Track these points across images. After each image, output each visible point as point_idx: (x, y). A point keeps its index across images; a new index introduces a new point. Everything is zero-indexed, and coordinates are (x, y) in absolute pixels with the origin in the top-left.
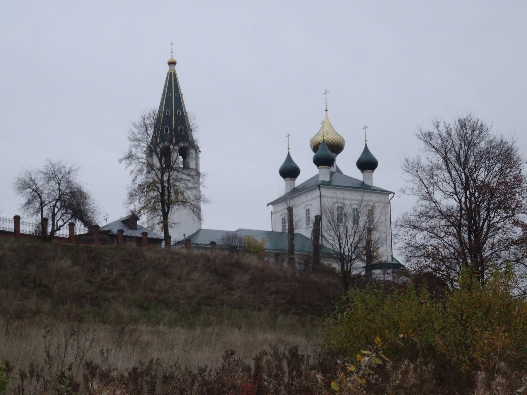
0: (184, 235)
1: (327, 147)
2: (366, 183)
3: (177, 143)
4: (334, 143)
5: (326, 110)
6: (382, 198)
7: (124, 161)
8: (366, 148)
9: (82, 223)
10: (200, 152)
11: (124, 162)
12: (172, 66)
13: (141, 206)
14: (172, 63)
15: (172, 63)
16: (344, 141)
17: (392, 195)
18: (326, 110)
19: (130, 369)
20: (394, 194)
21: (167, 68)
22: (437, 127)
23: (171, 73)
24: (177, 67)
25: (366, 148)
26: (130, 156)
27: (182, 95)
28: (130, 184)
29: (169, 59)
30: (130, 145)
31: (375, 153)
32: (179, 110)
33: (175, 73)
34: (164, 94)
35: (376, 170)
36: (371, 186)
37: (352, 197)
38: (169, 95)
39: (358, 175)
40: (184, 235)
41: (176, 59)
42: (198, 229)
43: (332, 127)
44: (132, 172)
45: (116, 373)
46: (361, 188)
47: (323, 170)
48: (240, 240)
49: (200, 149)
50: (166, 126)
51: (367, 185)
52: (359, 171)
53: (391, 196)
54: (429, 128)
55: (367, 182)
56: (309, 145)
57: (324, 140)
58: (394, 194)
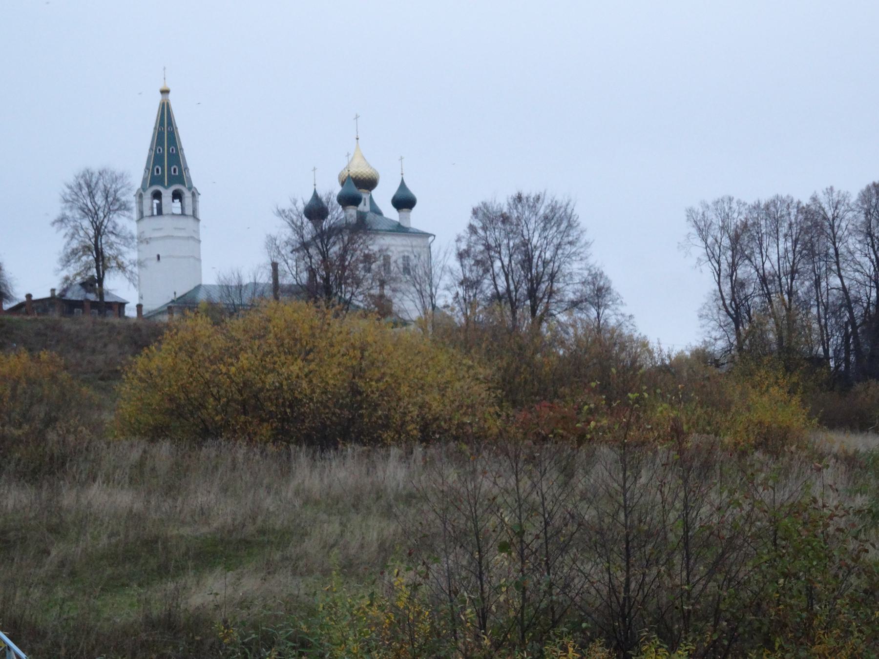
0: (175, 293)
1: (352, 183)
2: (402, 224)
3: (170, 183)
4: (360, 178)
5: (357, 139)
6: (417, 242)
7: (56, 224)
9: (326, 204)
12: (165, 95)
13: (75, 272)
14: (165, 92)
15: (165, 92)
18: (357, 139)
20: (434, 236)
21: (159, 97)
22: (295, 204)
24: (171, 97)
26: (62, 220)
27: (176, 128)
28: (62, 248)
29: (161, 86)
31: (414, 189)
32: (175, 166)
33: (168, 104)
35: (414, 209)
38: (159, 150)
39: (391, 213)
40: (175, 293)
41: (169, 86)
42: (197, 284)
43: (365, 159)
44: (65, 236)
45: (547, 369)
46: (397, 231)
49: (199, 192)
50: (157, 167)
51: (403, 227)
53: (431, 239)
55: (404, 224)
57: (349, 175)
58: (434, 236)
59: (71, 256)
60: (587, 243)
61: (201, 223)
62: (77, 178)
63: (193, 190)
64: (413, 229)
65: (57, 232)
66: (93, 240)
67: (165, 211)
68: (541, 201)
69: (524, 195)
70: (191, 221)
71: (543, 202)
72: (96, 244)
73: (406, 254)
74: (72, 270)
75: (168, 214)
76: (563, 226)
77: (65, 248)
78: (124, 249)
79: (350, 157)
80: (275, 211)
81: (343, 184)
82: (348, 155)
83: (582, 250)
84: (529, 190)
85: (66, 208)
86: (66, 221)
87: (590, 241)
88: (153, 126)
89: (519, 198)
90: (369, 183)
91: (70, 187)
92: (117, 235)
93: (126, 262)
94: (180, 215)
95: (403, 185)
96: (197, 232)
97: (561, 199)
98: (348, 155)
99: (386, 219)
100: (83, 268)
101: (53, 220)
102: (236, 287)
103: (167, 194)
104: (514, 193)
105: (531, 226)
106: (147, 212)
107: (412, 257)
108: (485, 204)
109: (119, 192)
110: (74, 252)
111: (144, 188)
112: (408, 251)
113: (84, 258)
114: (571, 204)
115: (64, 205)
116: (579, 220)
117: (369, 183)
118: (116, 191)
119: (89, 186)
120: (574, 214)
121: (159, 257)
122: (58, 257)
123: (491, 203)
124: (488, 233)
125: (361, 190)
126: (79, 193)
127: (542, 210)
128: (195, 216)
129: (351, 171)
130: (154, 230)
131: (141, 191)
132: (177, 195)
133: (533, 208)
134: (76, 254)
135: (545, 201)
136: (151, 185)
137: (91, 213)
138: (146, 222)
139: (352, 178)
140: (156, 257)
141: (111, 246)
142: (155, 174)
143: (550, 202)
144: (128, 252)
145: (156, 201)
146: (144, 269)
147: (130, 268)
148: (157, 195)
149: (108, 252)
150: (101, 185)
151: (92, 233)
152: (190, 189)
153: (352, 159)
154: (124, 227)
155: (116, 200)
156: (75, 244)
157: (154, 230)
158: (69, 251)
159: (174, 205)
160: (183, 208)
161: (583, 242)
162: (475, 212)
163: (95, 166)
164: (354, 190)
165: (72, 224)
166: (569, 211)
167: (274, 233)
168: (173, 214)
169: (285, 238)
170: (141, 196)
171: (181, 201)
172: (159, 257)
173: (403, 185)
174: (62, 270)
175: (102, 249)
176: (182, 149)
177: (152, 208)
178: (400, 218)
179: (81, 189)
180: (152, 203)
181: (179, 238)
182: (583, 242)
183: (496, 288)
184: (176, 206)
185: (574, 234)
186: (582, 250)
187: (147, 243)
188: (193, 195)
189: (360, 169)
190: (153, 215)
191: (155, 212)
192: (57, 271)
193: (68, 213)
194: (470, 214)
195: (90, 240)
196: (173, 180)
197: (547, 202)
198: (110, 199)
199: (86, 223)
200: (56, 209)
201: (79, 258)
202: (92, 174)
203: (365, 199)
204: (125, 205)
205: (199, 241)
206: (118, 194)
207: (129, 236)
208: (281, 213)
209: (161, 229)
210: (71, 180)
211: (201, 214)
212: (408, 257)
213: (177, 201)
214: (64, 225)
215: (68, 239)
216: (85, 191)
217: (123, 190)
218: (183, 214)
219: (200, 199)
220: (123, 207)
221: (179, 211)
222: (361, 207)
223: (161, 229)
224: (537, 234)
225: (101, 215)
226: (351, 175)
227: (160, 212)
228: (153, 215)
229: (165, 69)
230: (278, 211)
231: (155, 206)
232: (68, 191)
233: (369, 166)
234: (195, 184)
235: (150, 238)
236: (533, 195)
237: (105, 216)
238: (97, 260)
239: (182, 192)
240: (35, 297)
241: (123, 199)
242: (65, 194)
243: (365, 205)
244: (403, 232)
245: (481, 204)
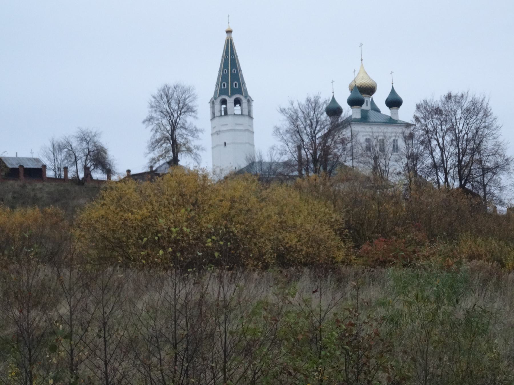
2: (392, 118)
3: (233, 94)
4: (363, 87)
5: (362, 60)
8: (393, 89)
10: (253, 101)
11: (146, 123)
13: (159, 155)
14: (229, 32)
15: (229, 32)
16: (376, 84)
17: (414, 127)
18: (362, 60)
19: (318, 261)
21: (225, 36)
22: (292, 104)
23: (228, 40)
24: (233, 35)
25: (393, 89)
26: (150, 119)
27: (237, 56)
29: (227, 28)
30: (149, 111)
31: (401, 94)
32: (236, 82)
33: (231, 40)
34: (223, 57)
35: (401, 107)
36: (397, 121)
37: (363, 129)
39: (386, 111)
41: (232, 28)
47: (355, 109)
48: (104, 161)
50: (224, 83)
51: (393, 120)
52: (388, 108)
54: (286, 105)
55: (394, 118)
56: (348, 87)
59: (156, 143)
60: (497, 127)
61: (254, 120)
62: (159, 91)
63: (248, 98)
64: (400, 121)
65: (146, 128)
66: (170, 132)
67: (229, 113)
68: (464, 99)
69: (453, 94)
70: (247, 119)
71: (466, 98)
72: (172, 135)
73: (368, 137)
74: (157, 153)
75: (231, 115)
76: (481, 115)
77: (151, 138)
78: (190, 138)
79: (356, 73)
80: (279, 109)
81: (351, 91)
82: (355, 71)
83: (494, 132)
84: (456, 91)
85: (152, 112)
86: (152, 120)
87: (500, 126)
88: (221, 55)
89: (449, 97)
90: (370, 90)
91: (154, 97)
92: (186, 129)
93: (192, 147)
94: (240, 115)
95: (393, 91)
96: (251, 126)
97: (478, 96)
98: (355, 71)
99: (382, 114)
100: (164, 152)
101: (143, 120)
102: (258, 162)
103: (230, 101)
104: (446, 93)
105: (458, 116)
106: (217, 114)
107: (372, 139)
108: (425, 101)
109: (187, 100)
110: (158, 141)
111: (215, 98)
112: (369, 135)
113: (164, 145)
114: (486, 100)
115: (150, 110)
116: (491, 112)
117: (370, 90)
118: (185, 99)
119: (167, 96)
120: (488, 107)
121: (225, 144)
122: (146, 145)
123: (430, 101)
124: (427, 121)
125: (363, 95)
126: (161, 102)
127: (466, 104)
128: (250, 116)
129: (357, 82)
130: (223, 125)
131: (213, 99)
132: (237, 102)
133: (458, 102)
134: (159, 143)
135: (468, 98)
136: (220, 94)
137: (169, 115)
138: (217, 120)
139: (358, 87)
140: (223, 143)
141: (182, 136)
142: (223, 87)
143: (471, 99)
144: (193, 141)
145: (224, 106)
146: (204, 152)
147: (195, 151)
148: (224, 102)
149: (180, 140)
150: (175, 96)
151: (169, 128)
152: (246, 96)
153: (358, 74)
154: (191, 124)
155: (185, 105)
156: (158, 136)
157: (223, 125)
158: (154, 140)
159: (235, 108)
160: (242, 110)
161: (495, 127)
162: (418, 107)
163: (171, 83)
164: (359, 95)
165: (156, 122)
166: (485, 105)
167: (279, 125)
168: (235, 114)
169: (285, 128)
170: (213, 103)
171: (240, 105)
172: (225, 144)
173: (393, 91)
174: (149, 153)
175: (176, 138)
176: (240, 70)
177: (221, 111)
178: (392, 114)
179: (162, 98)
180: (221, 108)
181: (238, 130)
182: (495, 127)
183: (433, 157)
184: (237, 109)
185: (488, 120)
186: (494, 132)
187: (218, 134)
188: (249, 101)
189: (362, 81)
190: (221, 115)
191: (223, 114)
192: (146, 154)
193: (154, 115)
194: (415, 108)
195: (168, 132)
196: (235, 91)
197: (469, 99)
198: (181, 105)
199: (165, 121)
200: (145, 112)
201: (161, 145)
202: (169, 88)
203: (367, 101)
204: (191, 109)
205: (253, 133)
206: (187, 102)
207: (194, 129)
208: (283, 111)
209: (227, 125)
210: (156, 92)
211: (254, 114)
212: (369, 139)
213: (238, 105)
214: (151, 123)
215: (154, 132)
216: (165, 99)
217: (190, 98)
218: (242, 115)
219: (254, 104)
220: (190, 110)
221: (239, 112)
222: (364, 107)
223: (227, 125)
224: (462, 122)
225: (176, 116)
226: (357, 85)
227: (226, 114)
228: (221, 115)
229: (229, 16)
230: (281, 110)
231: (223, 109)
232: (153, 100)
233: (370, 78)
234: (250, 93)
235: (220, 131)
236: (460, 95)
237: (178, 116)
238: (173, 146)
239: (241, 100)
240: (133, 172)
241: (190, 104)
242: (151, 101)
243: (367, 105)
244: (392, 123)
245: (422, 102)
